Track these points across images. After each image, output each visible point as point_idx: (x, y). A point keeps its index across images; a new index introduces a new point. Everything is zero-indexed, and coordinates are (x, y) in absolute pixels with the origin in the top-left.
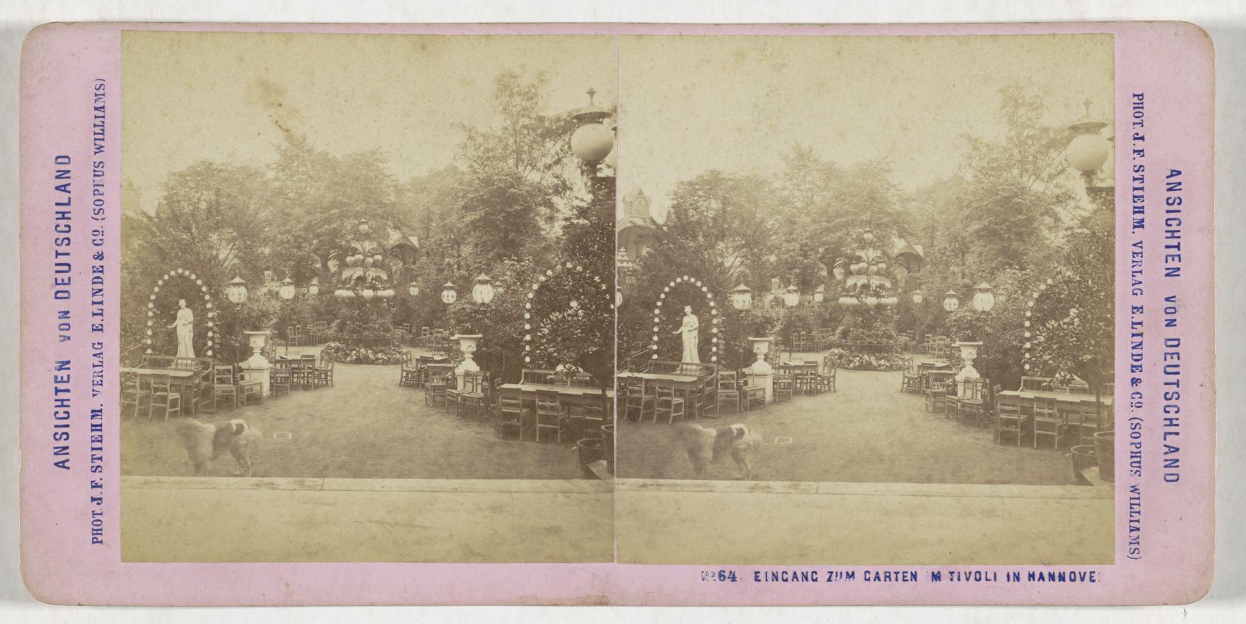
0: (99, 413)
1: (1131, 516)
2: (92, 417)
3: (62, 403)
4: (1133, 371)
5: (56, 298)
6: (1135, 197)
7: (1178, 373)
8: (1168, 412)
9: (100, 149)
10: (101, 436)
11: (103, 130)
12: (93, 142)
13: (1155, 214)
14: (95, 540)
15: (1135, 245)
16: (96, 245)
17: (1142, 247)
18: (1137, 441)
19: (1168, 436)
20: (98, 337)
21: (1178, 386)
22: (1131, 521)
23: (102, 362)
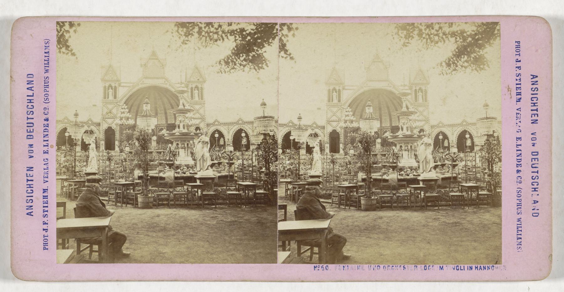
0: (517, 100)
1: (48, 59)
2: (43, 192)
3: (30, 186)
4: (517, 167)
5: (27, 138)
6: (517, 88)
7: (27, 123)
9: (519, 220)
12: (522, 223)
13: (38, 194)
14: (45, 248)
17: (44, 180)
18: (46, 93)
20: (46, 156)
23: (48, 167)
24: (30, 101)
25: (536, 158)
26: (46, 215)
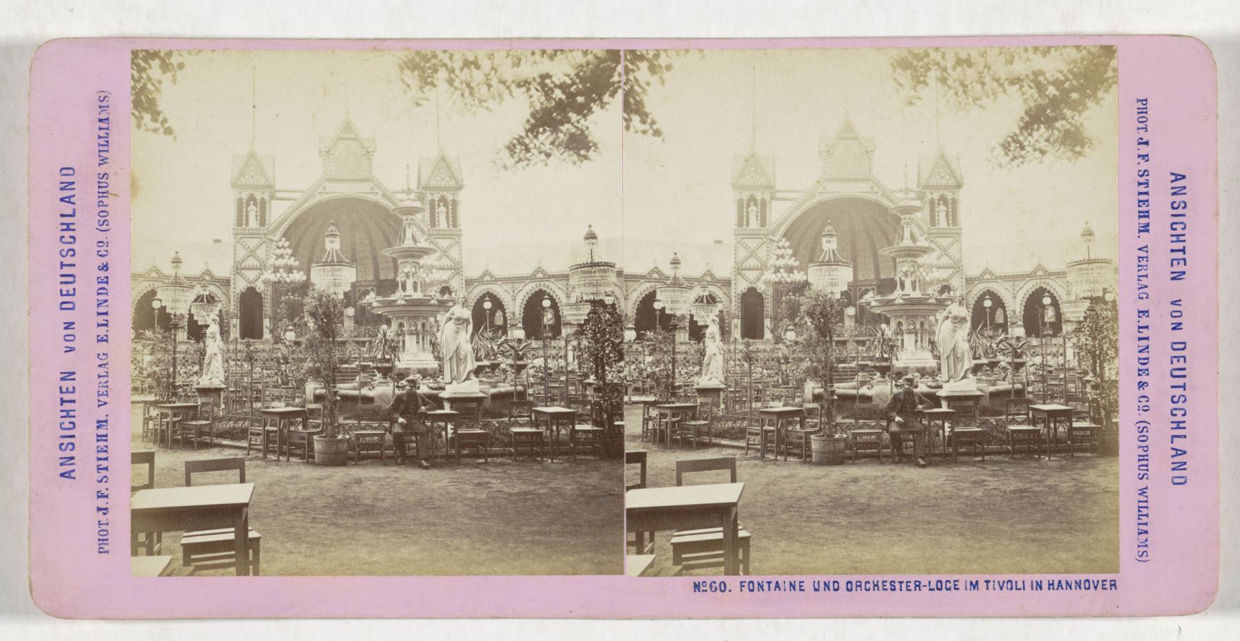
0: (105, 424)
2: (98, 427)
7: (62, 276)
8: (71, 237)
10: (1139, 206)
11: (1139, 511)
13: (86, 434)
14: (1144, 102)
15: (1140, 249)
16: (100, 256)
19: (1175, 439)
21: (1185, 389)
22: (108, 129)
23: (1139, 280)
24: (1178, 425)
25: (1182, 357)
26: (1141, 176)
